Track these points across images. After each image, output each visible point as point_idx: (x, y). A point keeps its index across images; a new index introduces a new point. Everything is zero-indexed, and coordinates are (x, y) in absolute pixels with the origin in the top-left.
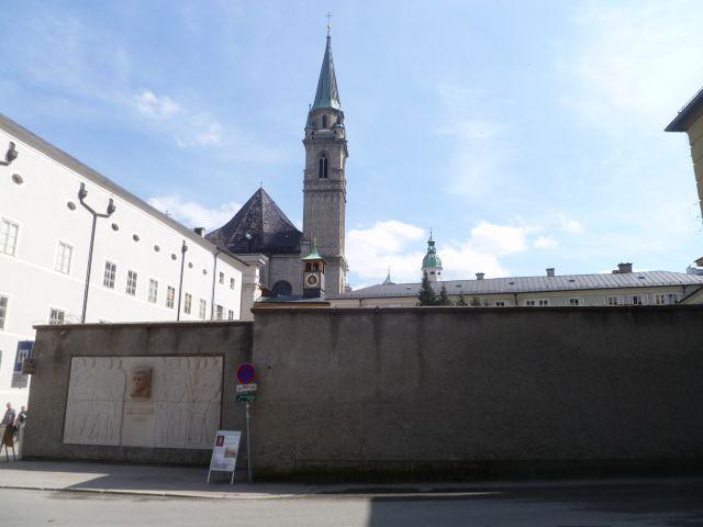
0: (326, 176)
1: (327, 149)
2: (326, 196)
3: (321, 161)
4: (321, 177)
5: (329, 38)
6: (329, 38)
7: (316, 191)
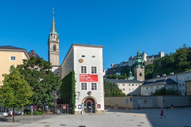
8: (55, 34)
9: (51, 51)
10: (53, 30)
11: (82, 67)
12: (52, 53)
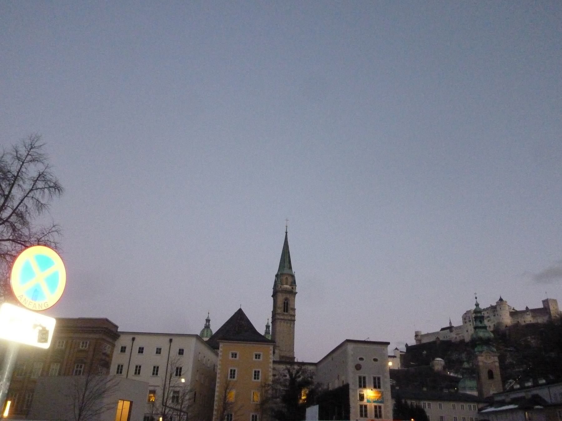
0: (287, 312)
1: (288, 296)
2: (287, 323)
3: (284, 303)
4: (284, 311)
5: (286, 233)
6: (286, 233)
7: (281, 319)
9: (279, 314)
10: (286, 264)
11: (360, 378)
12: (282, 317)
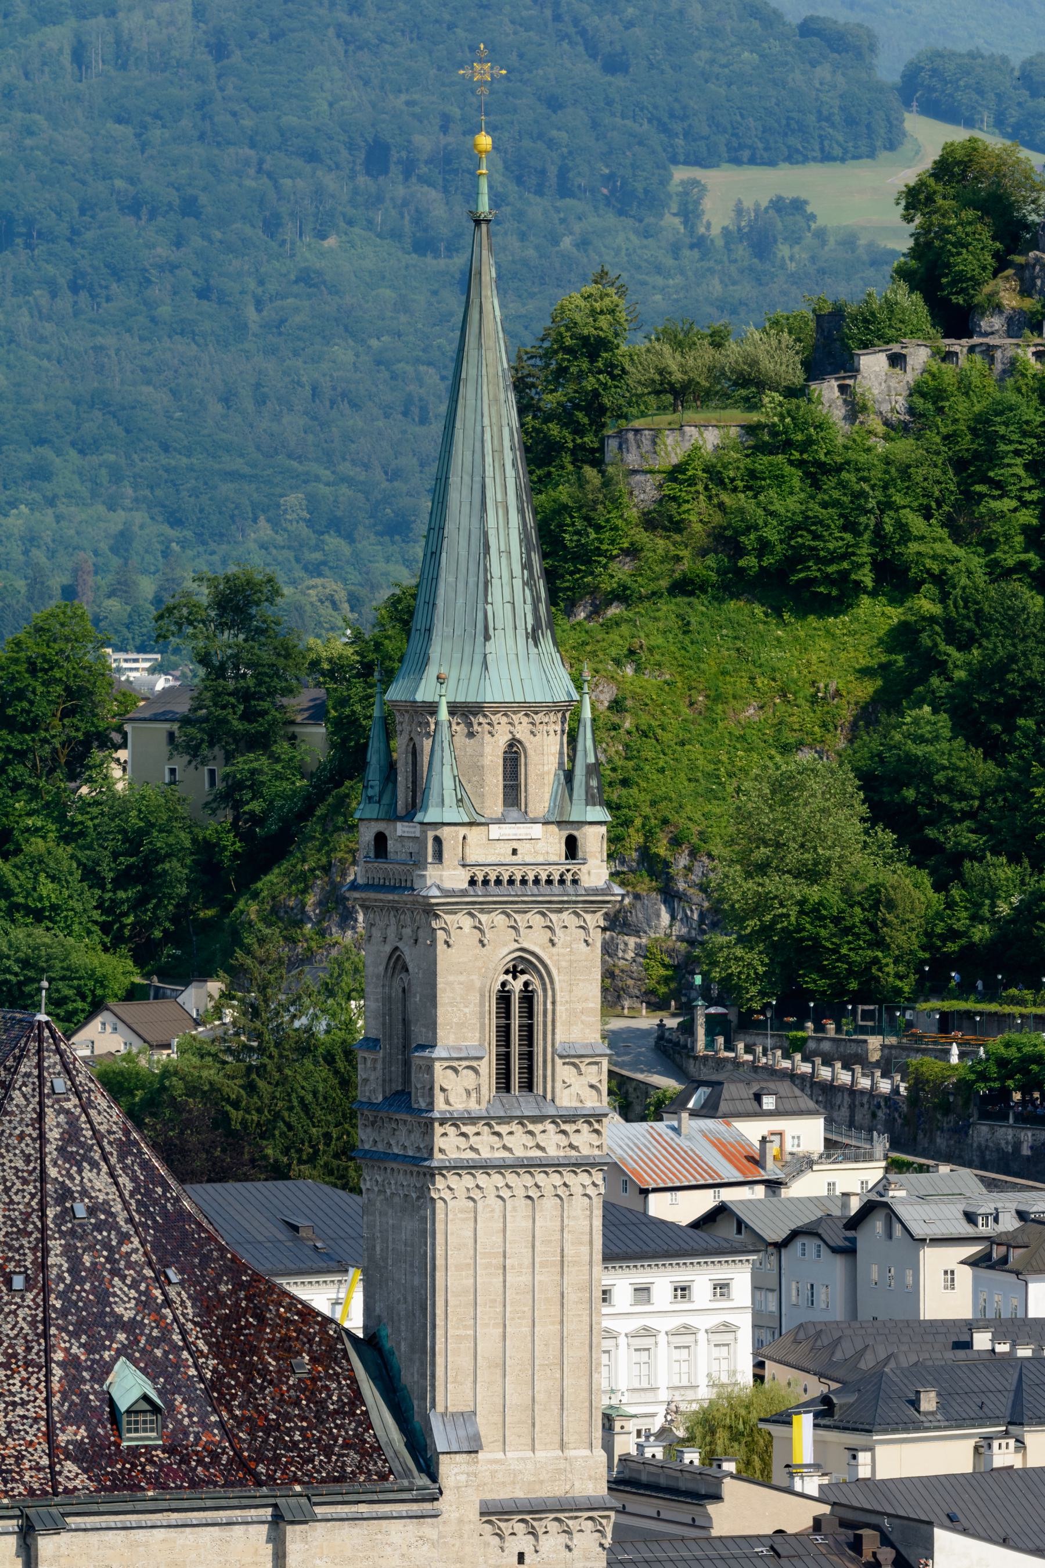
1: (535, 941)
3: (504, 998)
8: (530, 709)
